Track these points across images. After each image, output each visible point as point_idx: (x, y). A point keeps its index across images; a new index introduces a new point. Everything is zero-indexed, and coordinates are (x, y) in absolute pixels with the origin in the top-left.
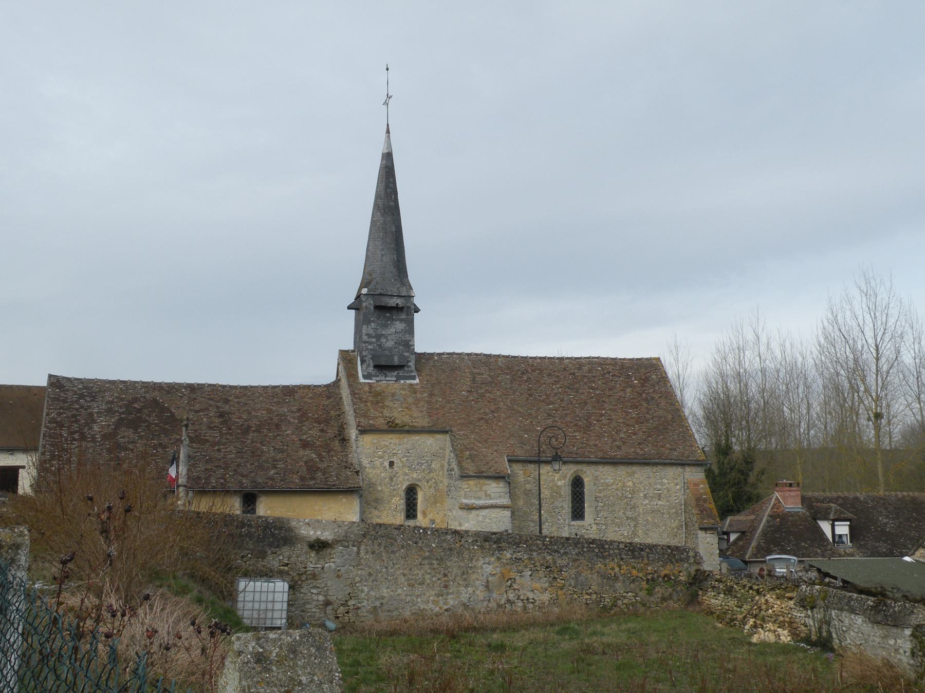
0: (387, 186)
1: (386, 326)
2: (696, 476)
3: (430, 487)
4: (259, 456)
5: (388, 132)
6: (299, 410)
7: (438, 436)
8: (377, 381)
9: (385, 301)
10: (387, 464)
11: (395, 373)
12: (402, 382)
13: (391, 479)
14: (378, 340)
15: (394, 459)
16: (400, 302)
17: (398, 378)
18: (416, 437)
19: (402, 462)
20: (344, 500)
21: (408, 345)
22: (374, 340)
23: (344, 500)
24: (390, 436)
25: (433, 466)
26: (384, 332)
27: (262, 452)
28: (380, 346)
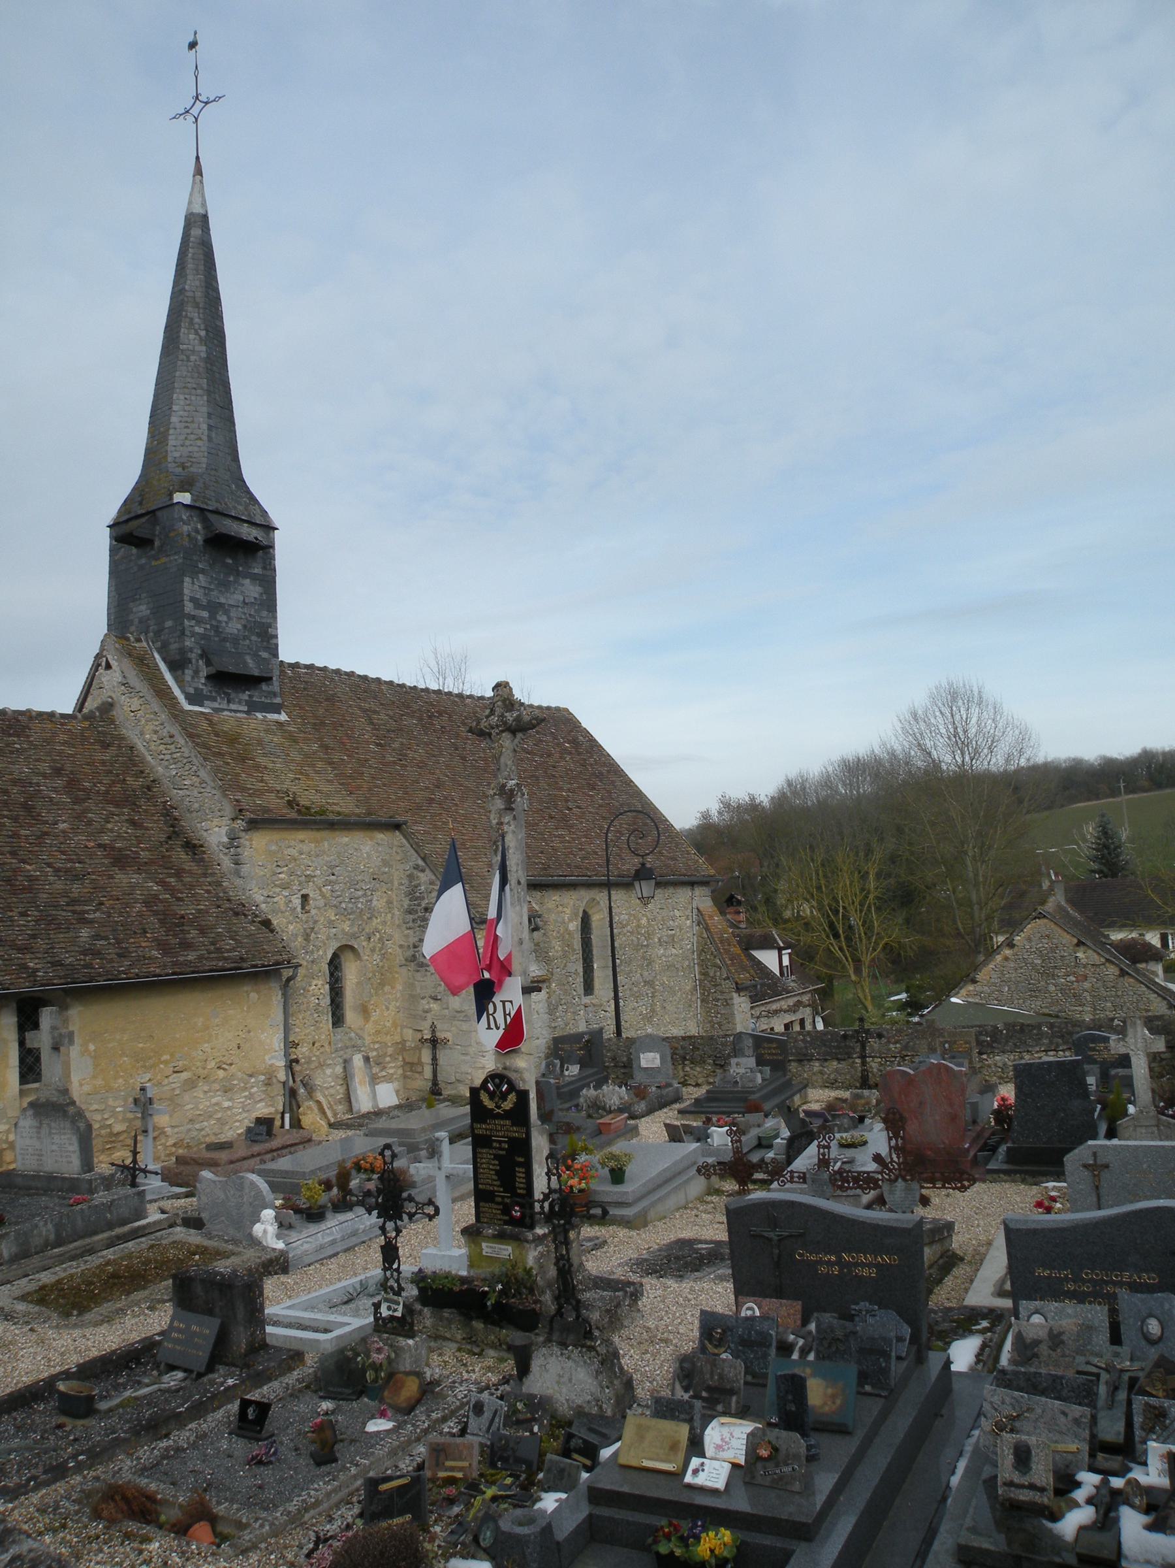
0: (194, 282)
1: (225, 586)
2: (702, 899)
3: (373, 950)
4: (29, 889)
5: (198, 171)
6: (58, 772)
7: (380, 836)
8: (216, 710)
9: (191, 543)
10: (297, 901)
11: (245, 696)
12: (259, 715)
13: (307, 938)
14: (213, 616)
15: (309, 890)
16: (248, 533)
17: (253, 707)
18: (344, 839)
19: (323, 896)
20: (251, 994)
21: (266, 636)
22: (205, 614)
23: (254, 996)
24: (301, 835)
25: (375, 903)
26: (223, 600)
27: (31, 879)
28: (216, 629)
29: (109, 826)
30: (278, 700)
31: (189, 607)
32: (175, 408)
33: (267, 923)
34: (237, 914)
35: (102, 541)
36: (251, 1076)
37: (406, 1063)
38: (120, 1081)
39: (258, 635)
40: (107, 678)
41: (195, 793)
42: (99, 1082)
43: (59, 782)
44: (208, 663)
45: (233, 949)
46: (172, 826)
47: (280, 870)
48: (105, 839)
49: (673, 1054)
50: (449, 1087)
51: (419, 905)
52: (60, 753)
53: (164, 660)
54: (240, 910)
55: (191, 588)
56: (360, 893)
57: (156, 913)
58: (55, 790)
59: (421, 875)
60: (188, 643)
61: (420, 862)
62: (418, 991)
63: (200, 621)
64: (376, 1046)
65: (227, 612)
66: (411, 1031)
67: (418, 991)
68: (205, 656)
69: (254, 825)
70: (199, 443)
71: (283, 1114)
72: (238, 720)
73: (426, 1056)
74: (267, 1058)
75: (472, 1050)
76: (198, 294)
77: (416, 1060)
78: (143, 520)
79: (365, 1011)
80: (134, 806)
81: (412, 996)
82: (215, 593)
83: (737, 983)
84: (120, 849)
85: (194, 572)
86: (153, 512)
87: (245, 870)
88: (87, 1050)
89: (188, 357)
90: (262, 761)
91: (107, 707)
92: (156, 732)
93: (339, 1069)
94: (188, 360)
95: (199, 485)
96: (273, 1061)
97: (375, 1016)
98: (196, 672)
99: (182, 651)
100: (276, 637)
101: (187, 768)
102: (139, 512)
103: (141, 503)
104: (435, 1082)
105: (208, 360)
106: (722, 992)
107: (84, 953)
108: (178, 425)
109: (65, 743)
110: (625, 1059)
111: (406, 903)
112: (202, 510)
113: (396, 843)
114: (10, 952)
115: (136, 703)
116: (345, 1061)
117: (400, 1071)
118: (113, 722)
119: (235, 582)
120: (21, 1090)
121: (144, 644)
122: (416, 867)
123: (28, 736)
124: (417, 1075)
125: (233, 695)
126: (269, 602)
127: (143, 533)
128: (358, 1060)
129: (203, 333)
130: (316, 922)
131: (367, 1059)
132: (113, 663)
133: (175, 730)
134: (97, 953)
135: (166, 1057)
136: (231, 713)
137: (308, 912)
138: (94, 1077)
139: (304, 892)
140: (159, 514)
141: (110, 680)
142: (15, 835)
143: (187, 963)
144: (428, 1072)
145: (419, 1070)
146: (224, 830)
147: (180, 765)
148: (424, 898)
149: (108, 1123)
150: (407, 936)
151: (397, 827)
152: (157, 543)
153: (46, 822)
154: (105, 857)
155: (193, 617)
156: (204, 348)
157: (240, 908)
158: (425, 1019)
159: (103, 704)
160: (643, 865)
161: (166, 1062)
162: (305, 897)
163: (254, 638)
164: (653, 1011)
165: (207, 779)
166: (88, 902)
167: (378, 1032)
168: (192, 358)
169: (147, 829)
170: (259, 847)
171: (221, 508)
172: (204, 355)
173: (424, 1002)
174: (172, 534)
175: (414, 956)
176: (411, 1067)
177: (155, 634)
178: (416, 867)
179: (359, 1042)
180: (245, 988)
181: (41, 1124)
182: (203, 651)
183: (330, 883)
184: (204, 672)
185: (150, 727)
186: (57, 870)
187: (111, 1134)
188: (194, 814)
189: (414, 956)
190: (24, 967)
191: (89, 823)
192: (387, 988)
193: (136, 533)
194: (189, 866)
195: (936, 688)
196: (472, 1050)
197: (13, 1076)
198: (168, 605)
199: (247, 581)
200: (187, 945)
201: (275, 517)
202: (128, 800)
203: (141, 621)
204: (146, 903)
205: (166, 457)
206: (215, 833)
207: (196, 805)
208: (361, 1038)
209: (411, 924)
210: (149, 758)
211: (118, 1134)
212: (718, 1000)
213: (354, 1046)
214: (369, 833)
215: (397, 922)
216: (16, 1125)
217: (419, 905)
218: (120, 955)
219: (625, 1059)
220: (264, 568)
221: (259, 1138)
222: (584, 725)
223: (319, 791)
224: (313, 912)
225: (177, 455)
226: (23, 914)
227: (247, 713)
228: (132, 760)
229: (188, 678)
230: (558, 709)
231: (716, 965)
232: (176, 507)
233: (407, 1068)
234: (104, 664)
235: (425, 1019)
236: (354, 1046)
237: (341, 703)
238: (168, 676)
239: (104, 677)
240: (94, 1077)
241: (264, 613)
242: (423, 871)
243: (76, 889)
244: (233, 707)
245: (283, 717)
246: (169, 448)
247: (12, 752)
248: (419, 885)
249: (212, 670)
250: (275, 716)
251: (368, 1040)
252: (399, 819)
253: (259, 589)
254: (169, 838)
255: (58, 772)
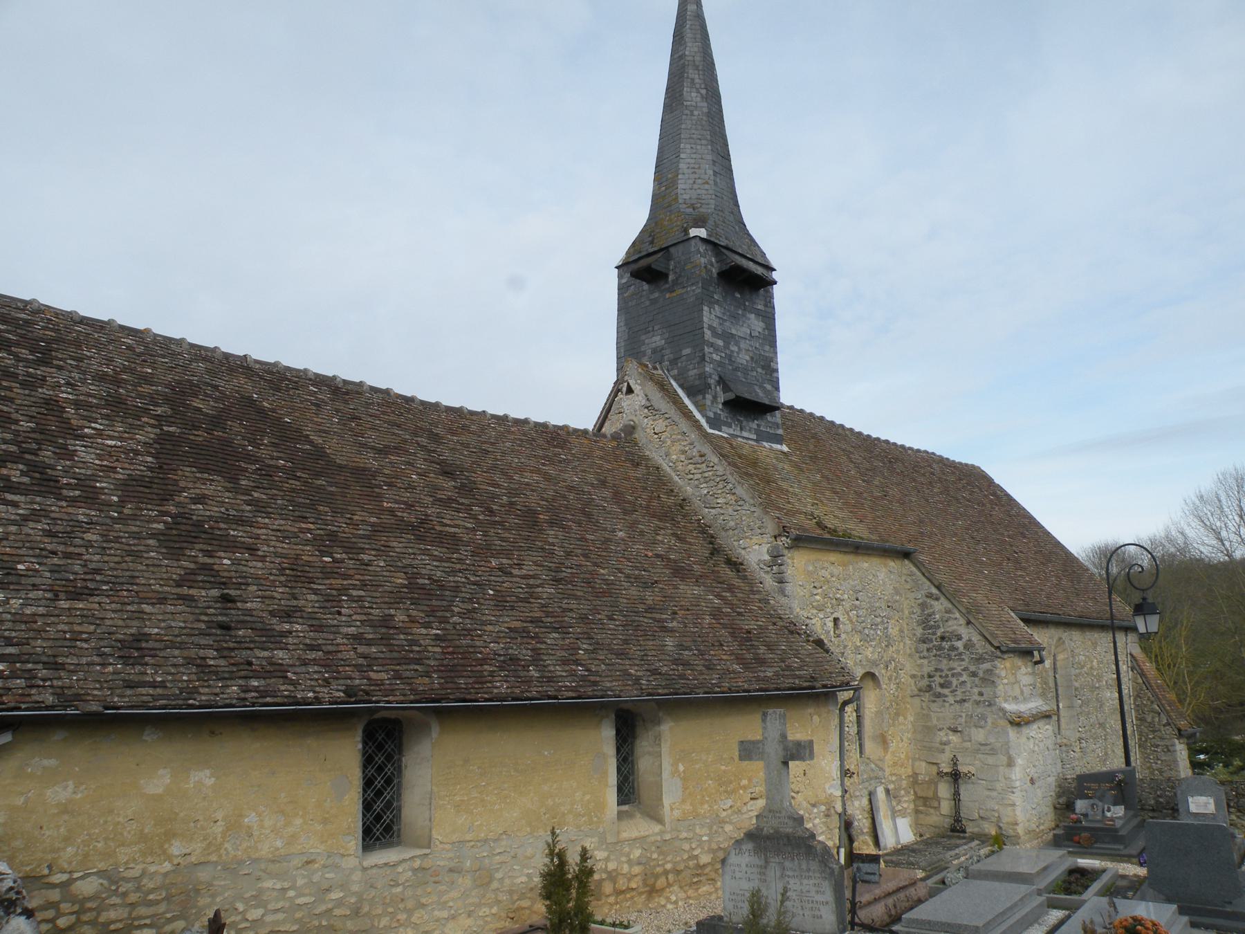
1: (735, 318)
11: (754, 425)
14: (727, 346)
17: (761, 437)
22: (720, 343)
24: (833, 557)
26: (734, 331)
28: (730, 357)
29: (659, 538)
30: (780, 432)
31: (708, 334)
32: (682, 156)
33: (819, 643)
34: (792, 632)
35: (611, 282)
36: (814, 806)
37: (917, 797)
38: (706, 806)
39: (763, 368)
40: (628, 402)
41: (730, 510)
42: (688, 807)
43: (607, 494)
44: (726, 389)
45: (799, 669)
46: (711, 543)
47: (815, 592)
48: (660, 550)
49: (1228, 801)
50: (971, 824)
51: (934, 634)
52: (600, 467)
53: (681, 386)
54: (792, 629)
55: (710, 316)
56: (879, 620)
57: (724, 626)
58: (604, 499)
59: (936, 603)
60: (708, 368)
61: (934, 591)
62: (935, 722)
63: (717, 349)
64: (894, 778)
65: (737, 344)
66: (924, 764)
67: (935, 722)
68: (722, 381)
69: (801, 542)
70: (706, 186)
71: (838, 848)
72: (752, 446)
73: (944, 790)
74: (827, 786)
75: (999, 786)
76: (698, 58)
77: (930, 794)
78: (660, 255)
79: (883, 741)
80: (675, 523)
81: (928, 728)
82: (727, 324)
83: (1179, 730)
84: (675, 561)
85: (711, 304)
86: (667, 248)
87: (789, 588)
88: (677, 770)
89: (692, 112)
90: (784, 485)
91: (630, 429)
92: (684, 452)
93: (865, 802)
94: (692, 115)
95: (711, 222)
96: (832, 791)
97: (893, 746)
98: (715, 397)
99: (703, 376)
100: (777, 371)
101: (721, 486)
102: (651, 250)
103: (652, 242)
104: (957, 819)
105: (709, 114)
106: (1162, 739)
107: (676, 662)
108: (686, 171)
109: (601, 458)
110: (1152, 802)
111: (919, 631)
112: (715, 245)
113: (905, 571)
114: (609, 656)
115: (660, 425)
116: (870, 794)
117: (912, 806)
118: (636, 444)
119: (743, 315)
120: (619, 813)
121: (660, 372)
122: (930, 596)
123: (570, 449)
124: (932, 811)
125: (745, 423)
126: (770, 337)
127: (659, 267)
128: (881, 794)
129: (704, 92)
130: (845, 647)
131: (887, 791)
132: (636, 388)
133: (707, 449)
134: (686, 664)
135: (745, 782)
136: (744, 436)
137: (839, 636)
138: (683, 801)
139: (835, 615)
140: (672, 250)
141: (631, 405)
142: (583, 539)
143: (766, 679)
144: (946, 807)
145: (936, 804)
146: (765, 548)
147: (712, 484)
148: (939, 627)
149: (696, 853)
150: (921, 666)
151: (906, 555)
152: (671, 277)
153: (605, 529)
154: (665, 567)
155: (712, 345)
156: (705, 104)
157: (792, 628)
158: (943, 751)
159: (626, 426)
160: (1144, 599)
161: (745, 788)
162: (836, 620)
163: (759, 370)
164: (1106, 754)
165: (745, 497)
166: (662, 610)
167: (895, 764)
168: (696, 113)
169: (690, 544)
170: (799, 564)
171: (731, 245)
172: (705, 110)
173: (942, 733)
174: (689, 266)
175: (930, 686)
176: (925, 802)
177: (670, 362)
178: (930, 596)
179: (880, 773)
180: (811, 710)
181: (767, 862)
182: (720, 377)
183: (855, 608)
184: (721, 399)
185: (677, 447)
186: (628, 576)
187: (698, 866)
188: (731, 532)
189: (930, 686)
190: (626, 673)
191: (642, 533)
192: (901, 718)
193: (645, 270)
194: (737, 582)
195: (1223, 474)
196: (999, 786)
197: (612, 796)
198: (686, 333)
199: (753, 316)
200: (762, 662)
201: (773, 260)
202: (666, 516)
203: (654, 351)
204: (713, 616)
205: (677, 198)
206: (756, 552)
207: (732, 524)
208: (882, 769)
209: (925, 653)
210: (676, 478)
211: (705, 866)
212: (1157, 746)
213: (876, 778)
214: (883, 560)
215: (908, 651)
216: (723, 861)
217: (934, 634)
218: (708, 668)
219: (1152, 802)
220: (766, 306)
221: (872, 877)
222: (997, 481)
223: (836, 518)
224: (843, 636)
225: (687, 197)
226: (611, 618)
227: (756, 441)
228: (658, 479)
229: (708, 403)
230: (973, 466)
231: (1153, 711)
232: (693, 242)
233: (920, 802)
234: (624, 389)
235: (943, 751)
236: (876, 778)
237: (820, 440)
238: (687, 401)
239: (625, 401)
240: (683, 801)
241: (767, 348)
242: (937, 599)
243: (650, 597)
244: (745, 434)
245: (785, 448)
246: (679, 191)
247: (560, 462)
248: (933, 613)
249: (731, 396)
250: (778, 447)
251: (888, 771)
252: (910, 547)
253: (761, 324)
254: (712, 554)
255: (603, 483)
